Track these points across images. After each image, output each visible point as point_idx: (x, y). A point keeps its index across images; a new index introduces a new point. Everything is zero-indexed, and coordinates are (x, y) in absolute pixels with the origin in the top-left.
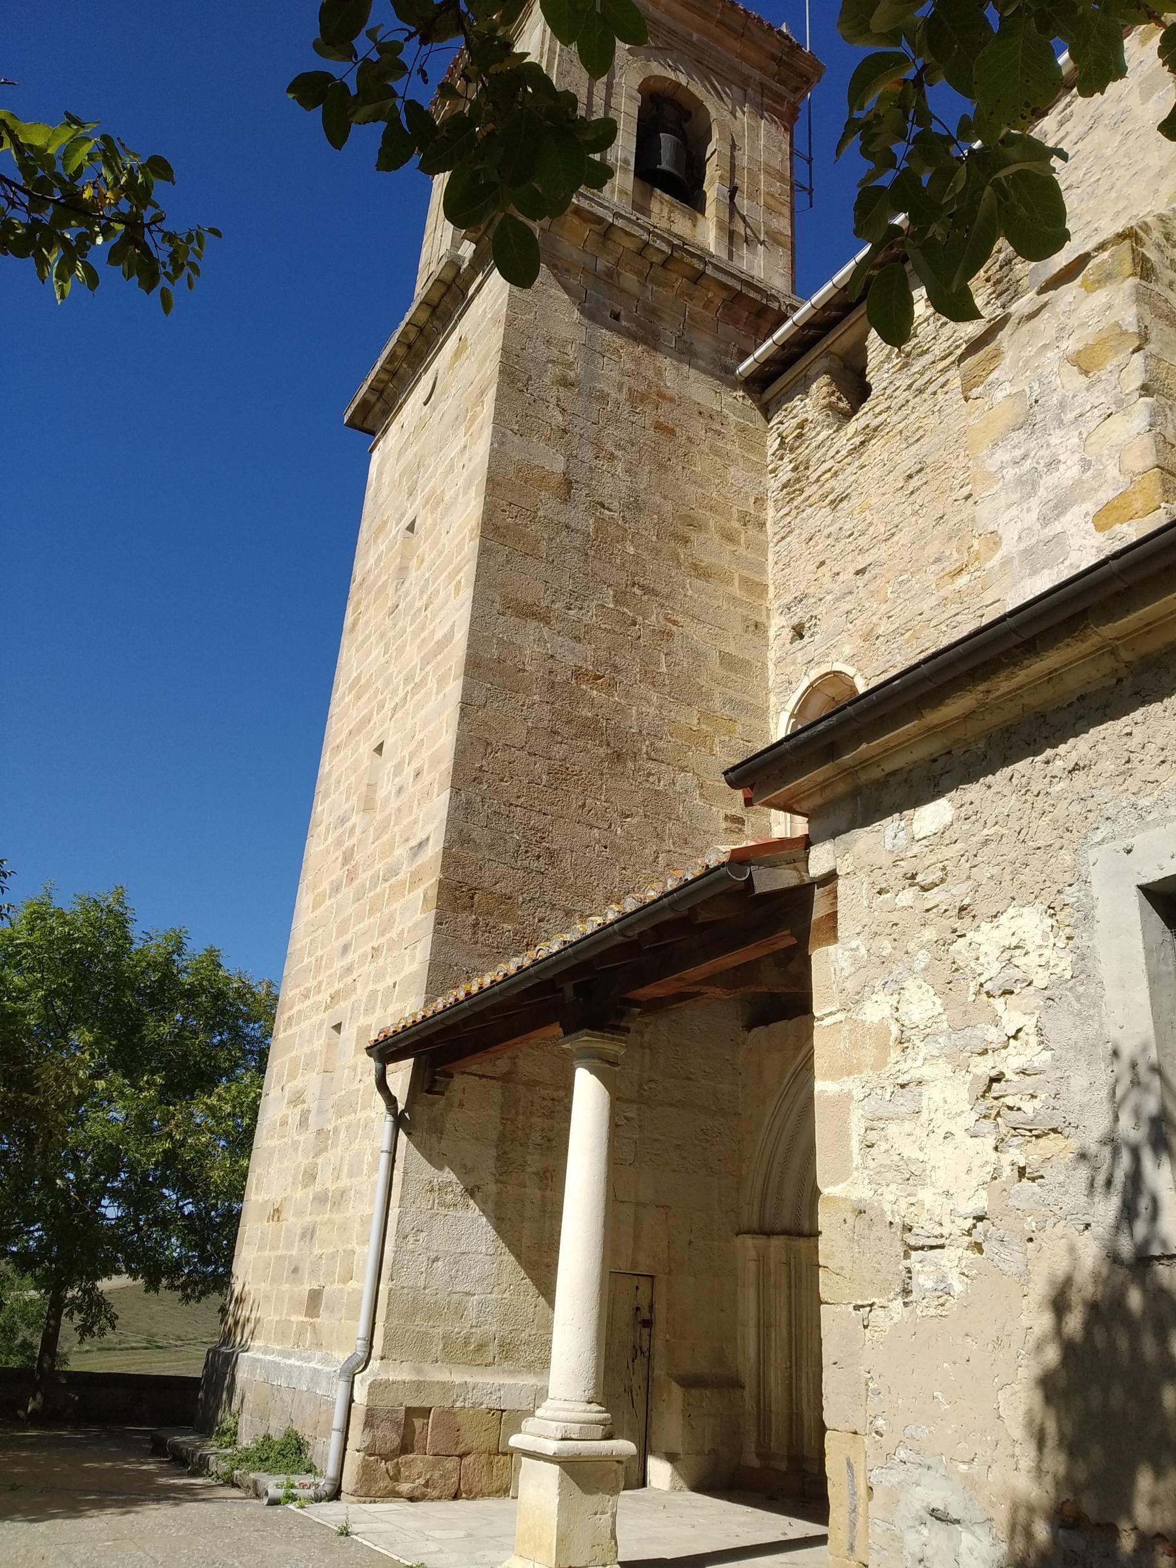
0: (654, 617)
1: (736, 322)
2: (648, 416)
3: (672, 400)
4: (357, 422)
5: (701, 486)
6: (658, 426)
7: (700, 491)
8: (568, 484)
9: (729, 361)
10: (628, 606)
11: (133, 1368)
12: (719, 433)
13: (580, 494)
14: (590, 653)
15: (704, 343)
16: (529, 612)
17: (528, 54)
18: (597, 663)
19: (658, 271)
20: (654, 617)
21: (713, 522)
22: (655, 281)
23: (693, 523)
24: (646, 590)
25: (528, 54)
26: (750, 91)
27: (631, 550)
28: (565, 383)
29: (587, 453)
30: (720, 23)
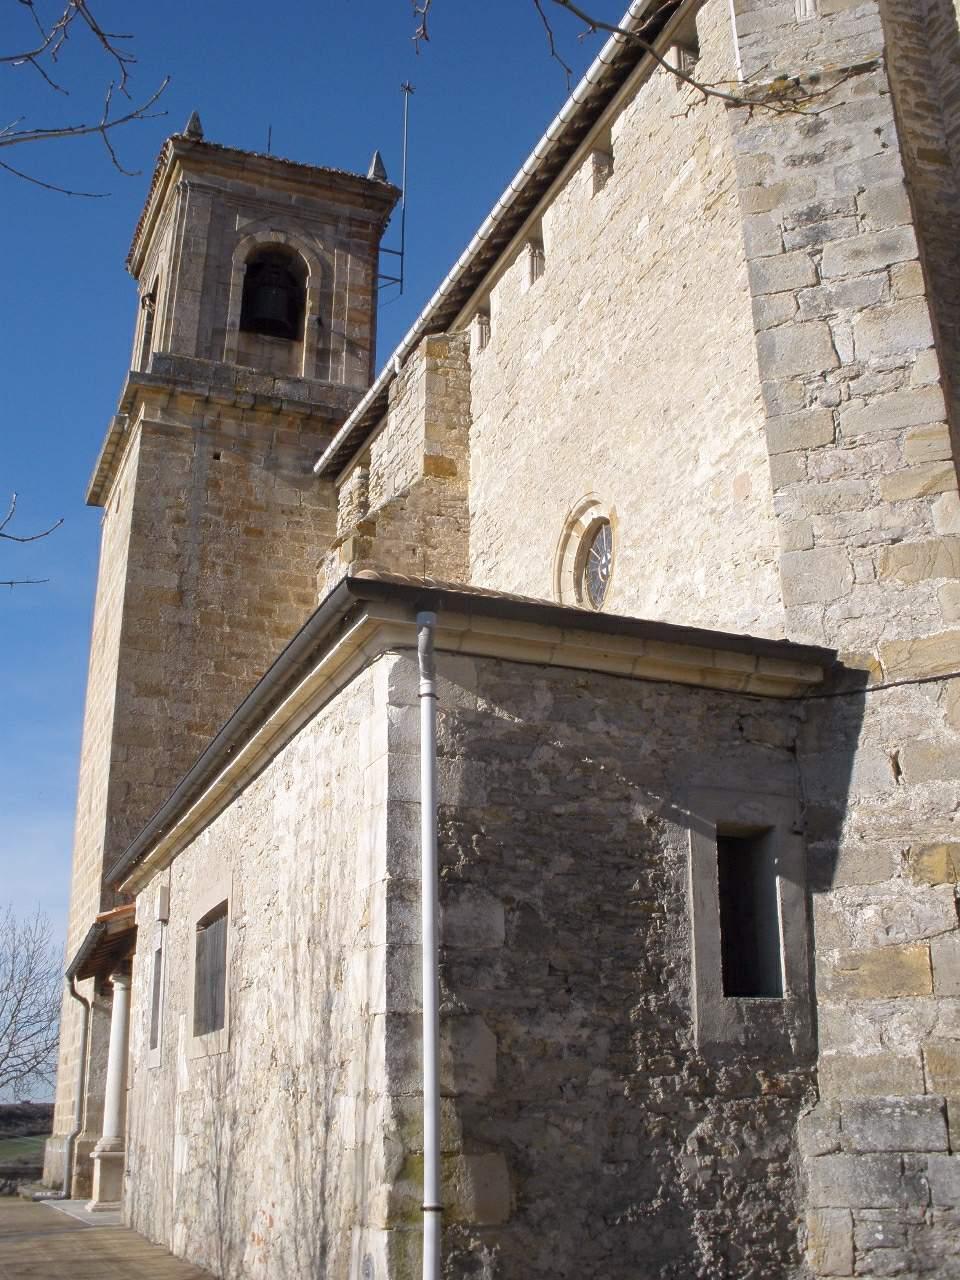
0: (245, 674)
1: (314, 430)
2: (240, 525)
3: (260, 508)
4: (93, 501)
5: (283, 568)
6: (248, 531)
7: (282, 571)
8: (181, 594)
9: (307, 463)
10: (225, 671)
11: (117, 600)
12: (298, 523)
13: (190, 599)
14: (197, 710)
15: (287, 458)
16: (155, 691)
17: (599, 185)
18: (203, 715)
19: (251, 414)
20: (245, 674)
21: (292, 591)
22: (247, 420)
23: (274, 596)
24: (241, 656)
25: (599, 185)
26: (341, 226)
27: (227, 629)
28: (179, 520)
29: (195, 568)
30: (311, 183)
